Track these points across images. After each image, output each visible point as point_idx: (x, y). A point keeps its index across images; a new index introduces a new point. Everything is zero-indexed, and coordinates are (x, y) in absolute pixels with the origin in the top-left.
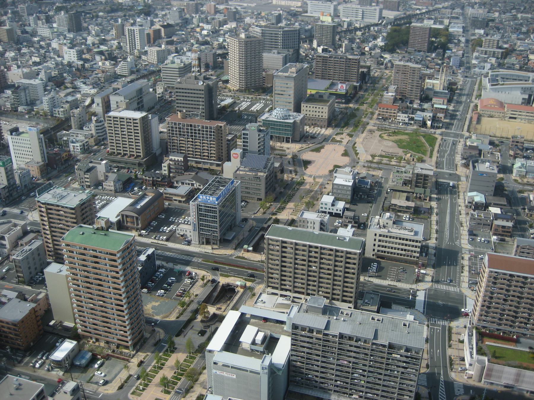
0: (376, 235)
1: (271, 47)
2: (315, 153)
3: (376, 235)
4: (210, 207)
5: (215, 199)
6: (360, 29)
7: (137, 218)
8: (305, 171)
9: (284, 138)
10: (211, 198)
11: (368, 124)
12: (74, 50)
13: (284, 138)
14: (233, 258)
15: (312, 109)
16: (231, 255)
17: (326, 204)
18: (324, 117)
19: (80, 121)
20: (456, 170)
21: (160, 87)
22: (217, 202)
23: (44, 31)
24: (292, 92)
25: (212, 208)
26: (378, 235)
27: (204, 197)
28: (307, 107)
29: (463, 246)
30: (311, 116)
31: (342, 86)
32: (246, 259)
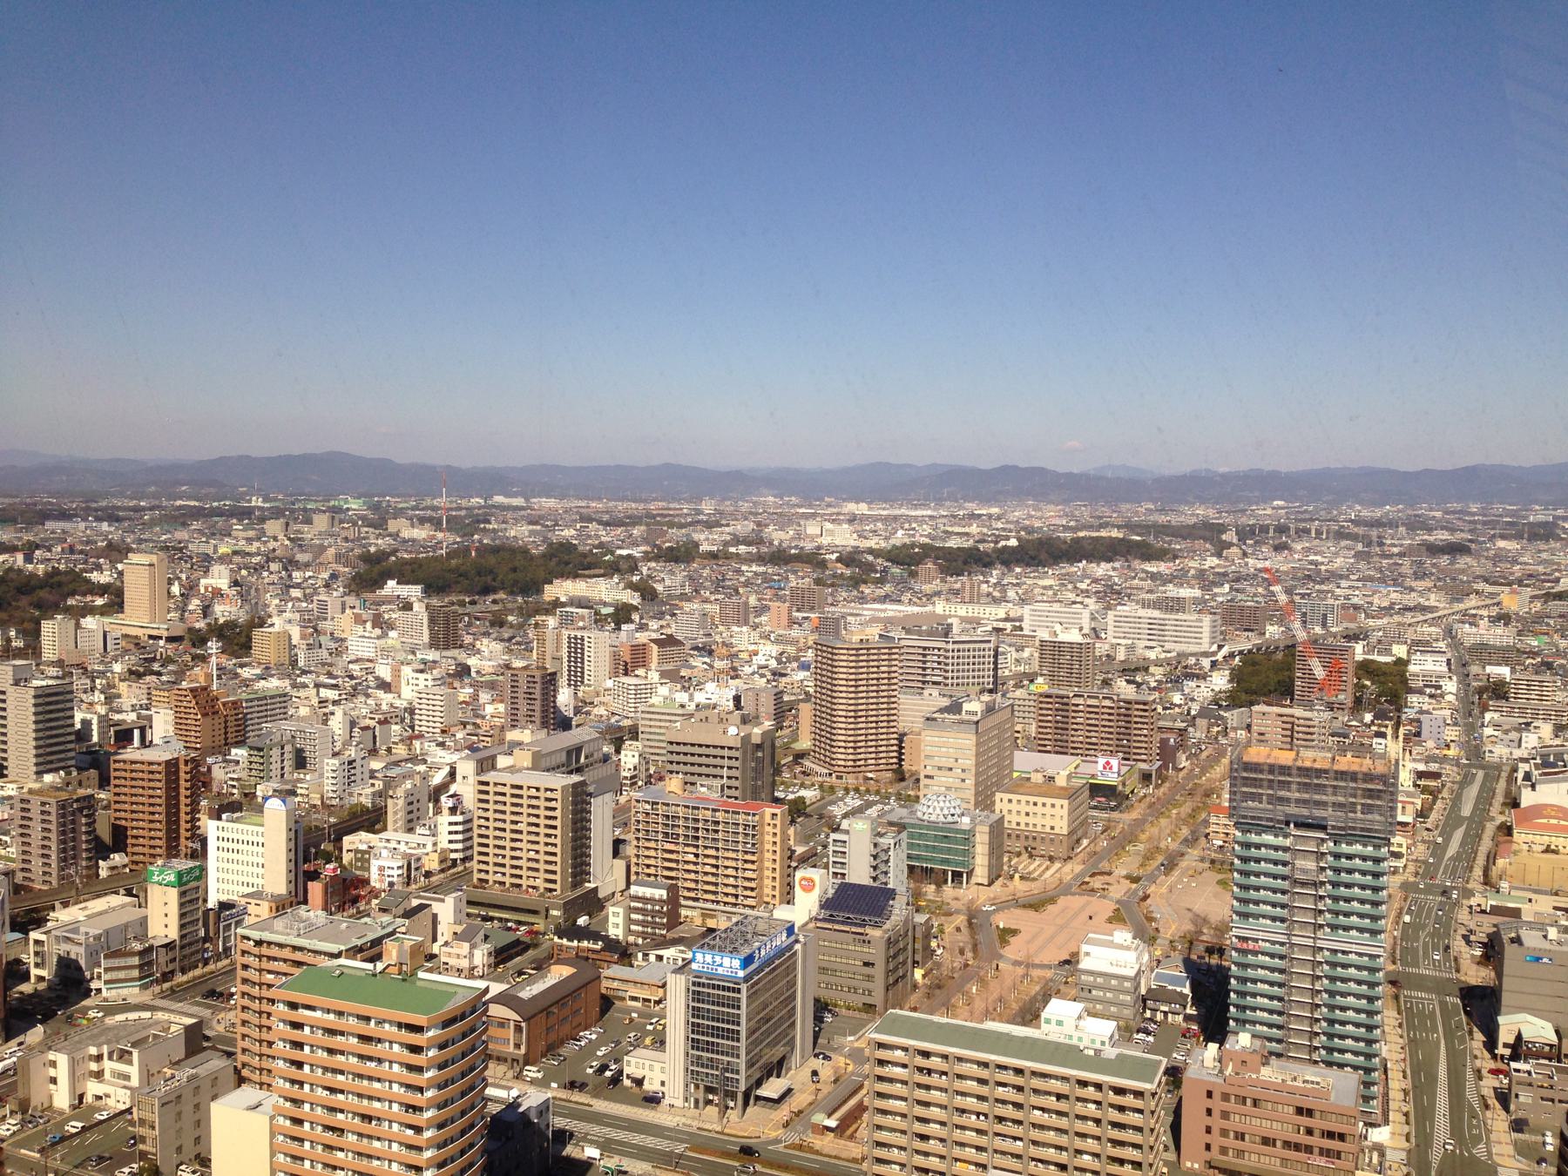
0: (1210, 1094)
1: (924, 682)
2: (1031, 913)
3: (1210, 1094)
4: (724, 988)
5: (736, 963)
6: (1158, 663)
7: (518, 1029)
8: (1001, 951)
9: (945, 872)
10: (727, 961)
11: (1182, 855)
12: (429, 677)
13: (945, 872)
14: (780, 1148)
15: (1024, 808)
16: (777, 1141)
17: (1060, 1023)
18: (1057, 831)
19: (410, 812)
20: (1458, 971)
21: (630, 754)
22: (741, 974)
23: (361, 643)
24: (969, 762)
25: (729, 989)
26: (1217, 1095)
27: (709, 958)
28: (1010, 801)
29: (1497, 1159)
30: (1023, 827)
31: (1108, 763)
32: (817, 1153)
